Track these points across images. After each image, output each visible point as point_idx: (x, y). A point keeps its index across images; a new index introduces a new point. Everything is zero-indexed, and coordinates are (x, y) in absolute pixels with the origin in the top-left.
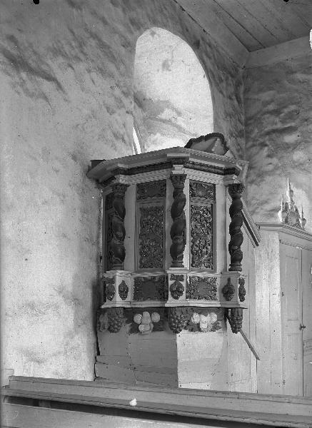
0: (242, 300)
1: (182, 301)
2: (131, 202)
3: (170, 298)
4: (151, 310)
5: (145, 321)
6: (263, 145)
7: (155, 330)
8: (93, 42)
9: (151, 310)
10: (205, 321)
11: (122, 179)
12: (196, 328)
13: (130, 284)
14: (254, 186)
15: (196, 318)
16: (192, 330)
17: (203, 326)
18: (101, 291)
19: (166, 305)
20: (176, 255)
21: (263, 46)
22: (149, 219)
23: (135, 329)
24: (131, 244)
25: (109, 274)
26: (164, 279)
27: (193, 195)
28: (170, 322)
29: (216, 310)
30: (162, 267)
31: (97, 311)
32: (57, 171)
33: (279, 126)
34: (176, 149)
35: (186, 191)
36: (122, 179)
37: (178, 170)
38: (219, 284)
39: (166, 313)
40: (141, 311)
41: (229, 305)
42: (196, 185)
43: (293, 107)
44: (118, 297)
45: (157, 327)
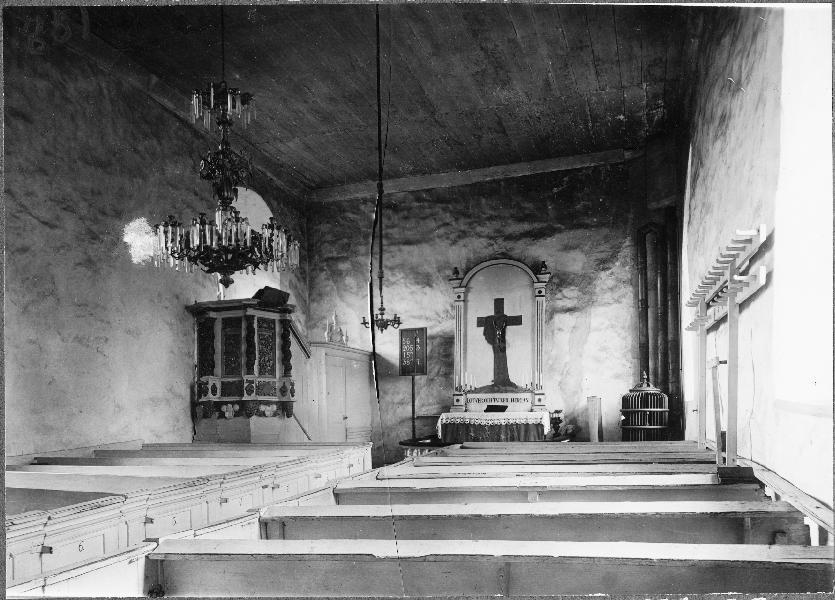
0: (293, 396)
1: (253, 397)
2: (218, 328)
3: (246, 395)
4: (233, 403)
5: (229, 411)
6: (322, 270)
7: (235, 416)
8: (189, 210)
9: (233, 403)
10: (269, 410)
11: (212, 315)
12: (263, 414)
13: (219, 386)
14: (315, 304)
15: (263, 408)
16: (260, 416)
17: (267, 413)
18: (198, 390)
19: (244, 399)
20: (250, 371)
21: (319, 187)
22: (231, 343)
23: (222, 415)
24: (218, 358)
25: (203, 379)
26: (242, 382)
27: (259, 327)
28: (246, 410)
29: (276, 403)
30: (240, 375)
31: (194, 405)
32: (167, 308)
33: (335, 254)
34: (248, 300)
35: (255, 326)
36: (212, 315)
37: (250, 312)
38: (278, 385)
39: (242, 404)
40: (226, 403)
41: (284, 399)
42: (261, 320)
43: (345, 240)
44: (210, 395)
45: (237, 414)
